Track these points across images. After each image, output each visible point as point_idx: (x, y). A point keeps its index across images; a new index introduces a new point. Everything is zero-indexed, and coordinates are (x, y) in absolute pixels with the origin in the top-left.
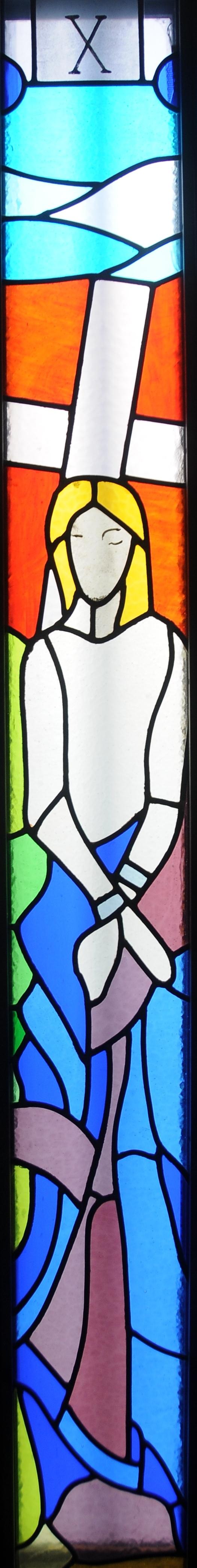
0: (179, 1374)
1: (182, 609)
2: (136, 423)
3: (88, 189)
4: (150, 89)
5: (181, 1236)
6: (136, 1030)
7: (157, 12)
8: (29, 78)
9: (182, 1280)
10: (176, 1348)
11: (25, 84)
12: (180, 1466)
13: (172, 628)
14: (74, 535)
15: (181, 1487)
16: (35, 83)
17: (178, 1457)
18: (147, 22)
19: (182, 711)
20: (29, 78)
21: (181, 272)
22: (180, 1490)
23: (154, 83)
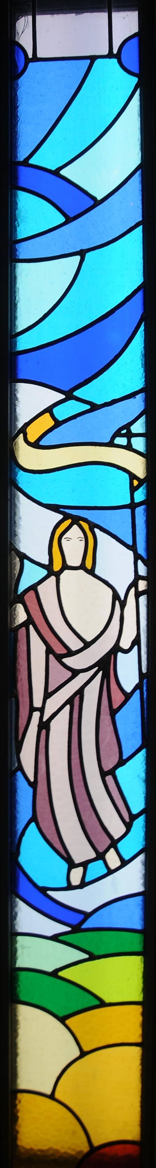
0: (17, 250)
1: (16, 781)
2: (99, 198)
3: (88, 407)
4: (115, 61)
5: (8, 384)
6: (77, 700)
7: (124, 5)
8: (30, 56)
9: (18, 1111)
10: (136, 70)
11: (28, 61)
12: (17, 204)
13: (137, 557)
14: (82, 541)
15: (15, 559)
16: (36, 59)
17: (144, 771)
18: (115, 15)
19: (20, 250)
20: (30, 56)
21: (11, 383)
22: (16, 556)
23: (118, 56)
